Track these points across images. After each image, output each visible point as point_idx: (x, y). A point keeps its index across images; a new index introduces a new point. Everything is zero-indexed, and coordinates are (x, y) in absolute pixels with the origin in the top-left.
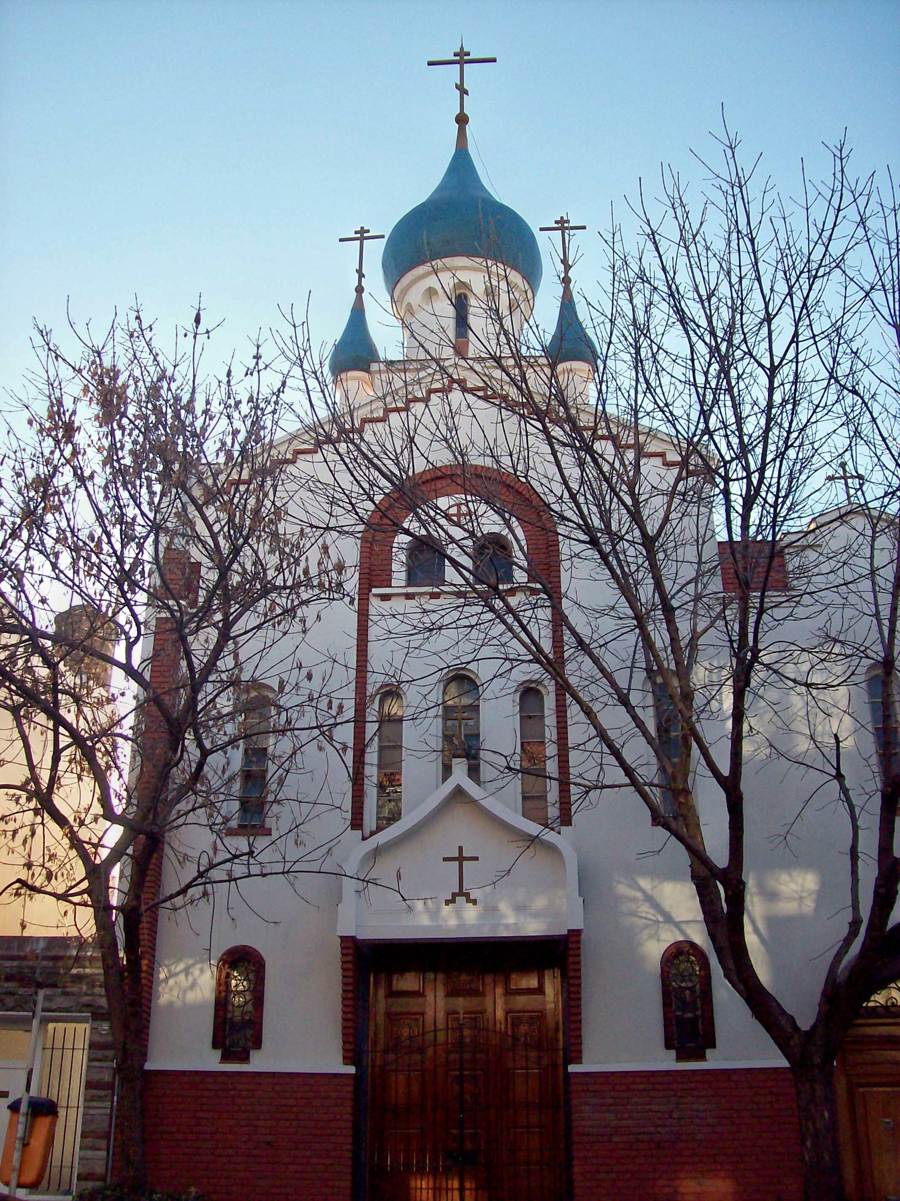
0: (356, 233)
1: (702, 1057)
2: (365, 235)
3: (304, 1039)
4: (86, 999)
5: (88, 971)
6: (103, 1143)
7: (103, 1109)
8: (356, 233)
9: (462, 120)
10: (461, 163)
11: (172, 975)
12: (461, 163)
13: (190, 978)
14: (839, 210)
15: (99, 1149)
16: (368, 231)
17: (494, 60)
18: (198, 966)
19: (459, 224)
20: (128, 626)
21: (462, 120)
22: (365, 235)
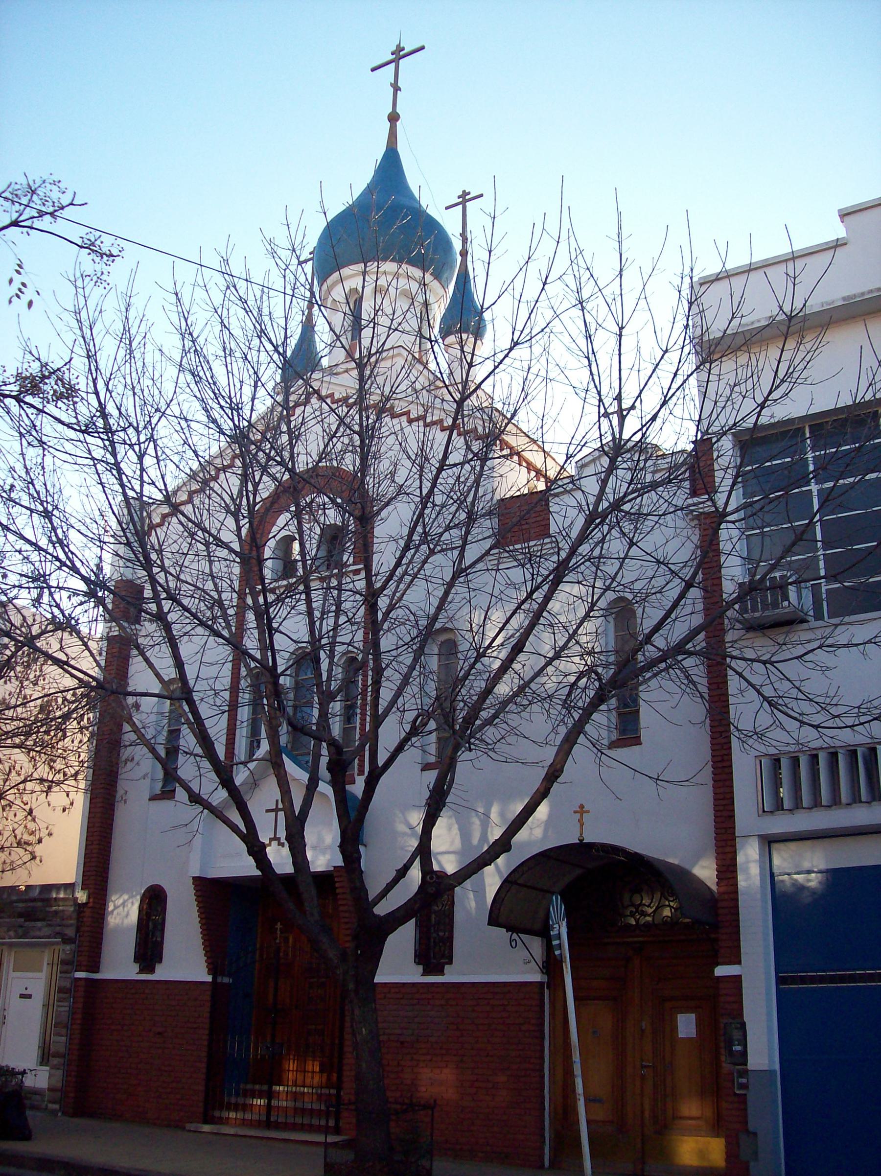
0: (459, 197)
1: (441, 972)
2: (467, 197)
3: (185, 960)
4: (58, 929)
5: (61, 908)
6: (64, 1031)
7: (65, 1008)
8: (459, 197)
9: (394, 118)
10: (390, 167)
11: (116, 908)
12: (390, 167)
13: (126, 909)
14: (795, 278)
15: (62, 1036)
16: (469, 193)
17: (423, 48)
18: (130, 901)
19: (387, 225)
20: (40, 689)
21: (394, 118)
22: (467, 197)
